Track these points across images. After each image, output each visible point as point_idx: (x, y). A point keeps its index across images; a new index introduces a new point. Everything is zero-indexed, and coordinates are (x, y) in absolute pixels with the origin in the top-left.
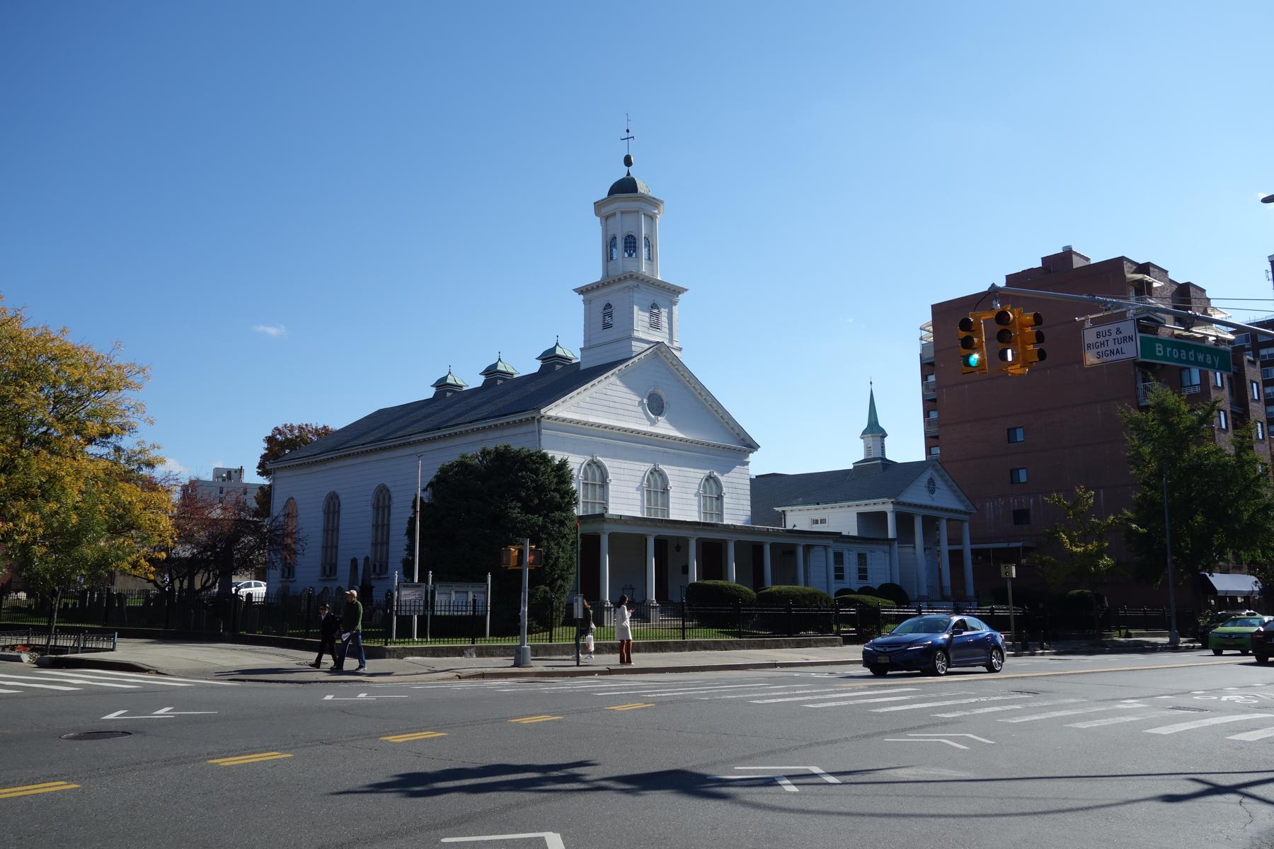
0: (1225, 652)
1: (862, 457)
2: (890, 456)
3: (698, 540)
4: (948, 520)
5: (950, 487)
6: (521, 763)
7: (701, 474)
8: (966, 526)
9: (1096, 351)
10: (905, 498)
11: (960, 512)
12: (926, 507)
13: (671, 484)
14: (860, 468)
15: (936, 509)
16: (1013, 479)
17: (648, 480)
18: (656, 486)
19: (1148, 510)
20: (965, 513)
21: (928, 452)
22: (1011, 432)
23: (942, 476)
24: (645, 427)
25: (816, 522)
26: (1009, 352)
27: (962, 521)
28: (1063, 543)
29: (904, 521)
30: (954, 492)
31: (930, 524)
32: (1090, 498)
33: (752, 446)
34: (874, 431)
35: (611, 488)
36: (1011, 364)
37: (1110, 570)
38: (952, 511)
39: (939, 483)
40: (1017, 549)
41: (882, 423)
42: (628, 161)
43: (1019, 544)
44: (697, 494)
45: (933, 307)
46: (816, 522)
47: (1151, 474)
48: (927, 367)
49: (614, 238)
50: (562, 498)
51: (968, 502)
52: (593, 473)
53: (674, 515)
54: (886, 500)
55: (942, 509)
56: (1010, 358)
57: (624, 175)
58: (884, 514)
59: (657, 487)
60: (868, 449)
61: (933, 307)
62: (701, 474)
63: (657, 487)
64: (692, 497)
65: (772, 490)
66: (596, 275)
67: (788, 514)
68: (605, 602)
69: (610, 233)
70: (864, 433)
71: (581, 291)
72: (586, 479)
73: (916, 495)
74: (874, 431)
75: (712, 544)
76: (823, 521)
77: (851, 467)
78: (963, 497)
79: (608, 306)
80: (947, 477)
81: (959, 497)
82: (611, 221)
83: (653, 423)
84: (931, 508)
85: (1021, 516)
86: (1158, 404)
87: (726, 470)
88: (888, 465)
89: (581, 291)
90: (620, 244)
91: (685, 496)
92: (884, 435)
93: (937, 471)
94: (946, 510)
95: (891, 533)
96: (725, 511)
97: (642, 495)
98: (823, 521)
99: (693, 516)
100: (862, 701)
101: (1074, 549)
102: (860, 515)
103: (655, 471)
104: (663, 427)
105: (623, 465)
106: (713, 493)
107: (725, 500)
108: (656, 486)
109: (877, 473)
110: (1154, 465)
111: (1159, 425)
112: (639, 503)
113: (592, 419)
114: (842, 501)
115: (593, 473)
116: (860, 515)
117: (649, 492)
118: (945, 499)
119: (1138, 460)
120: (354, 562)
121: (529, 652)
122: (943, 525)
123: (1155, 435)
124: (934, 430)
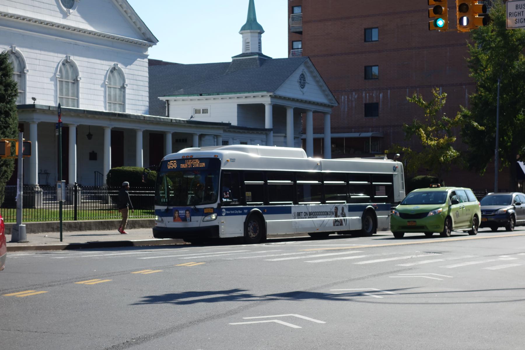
1: (240, 52)
2: (265, 52)
3: (145, 133)
4: (314, 112)
5: (317, 82)
6: (205, 291)
7: (106, 65)
8: (328, 118)
9: (514, 18)
10: (281, 92)
11: (324, 105)
12: (297, 100)
13: (80, 75)
14: (239, 63)
16: (367, 74)
17: (61, 71)
18: (67, 77)
19: (483, 109)
20: (328, 106)
21: (291, 47)
22: (367, 31)
23: (311, 72)
24: (58, 20)
25: (197, 111)
26: (465, 19)
27: (325, 113)
28: (420, 137)
29: (279, 113)
30: (320, 87)
31: (299, 113)
32: (441, 97)
33: (152, 40)
34: (253, 27)
35: (81, 85)
36: (465, 27)
37: (455, 160)
38: (317, 104)
40: (367, 138)
41: (259, 20)
43: (369, 134)
44: (104, 85)
46: (197, 111)
47: (487, 78)
50: (6, 90)
51: (331, 97)
52: (67, 72)
53: (83, 106)
54: (265, 93)
55: (310, 103)
56: (465, 23)
58: (261, 107)
59: (68, 77)
60: (246, 44)
62: (106, 65)
63: (68, 77)
64: (99, 87)
65: (168, 78)
67: (172, 104)
68: (35, 186)
70: (244, 28)
72: (62, 77)
73: (290, 89)
74: (253, 27)
75: (121, 132)
76: (205, 111)
77: (230, 60)
78: (328, 92)
80: (316, 73)
81: (324, 91)
83: (65, 15)
85: (371, 109)
86: (498, 18)
87: (128, 62)
88: (264, 60)
91: (93, 87)
92: (260, 31)
93: (308, 67)
94: (293, 100)
95: (268, 124)
96: (127, 101)
97: (56, 85)
98: (205, 111)
99: (100, 107)
100: (339, 259)
101: (430, 142)
102: (241, 107)
103: (67, 62)
104: (75, 20)
105: (39, 57)
106: (116, 82)
107: (127, 91)
108: (67, 77)
109: (250, 69)
110: (490, 70)
111: (498, 36)
112: (53, 93)
113: (11, 11)
114: (223, 92)
115: (67, 72)
116: (241, 107)
117: (61, 82)
118: (314, 93)
119: (476, 64)
121: (25, 230)
122: (310, 117)
123: (493, 45)
124: (298, 26)
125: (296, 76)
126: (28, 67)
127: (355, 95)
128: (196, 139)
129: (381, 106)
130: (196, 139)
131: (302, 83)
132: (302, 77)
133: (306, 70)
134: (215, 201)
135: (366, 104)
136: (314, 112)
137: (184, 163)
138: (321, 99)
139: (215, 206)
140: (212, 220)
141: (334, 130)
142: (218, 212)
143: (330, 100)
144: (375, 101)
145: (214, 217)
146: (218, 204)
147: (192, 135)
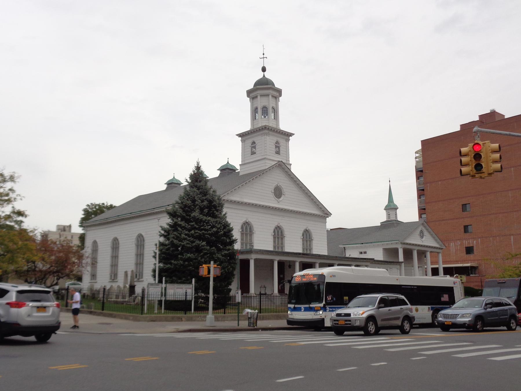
0: (451, 330)
2: (399, 219)
4: (431, 252)
12: (419, 245)
14: (385, 225)
15: (424, 246)
20: (440, 248)
21: (420, 217)
27: (438, 253)
29: (408, 254)
33: (326, 214)
38: (432, 247)
39: (426, 233)
42: (264, 70)
43: (468, 265)
45: (422, 141)
46: (361, 253)
48: (420, 173)
49: (257, 108)
57: (262, 76)
61: (422, 141)
63: (279, 234)
66: (247, 127)
69: (255, 106)
71: (241, 135)
73: (415, 240)
76: (365, 253)
79: (254, 143)
82: (255, 100)
84: (422, 246)
85: (469, 250)
89: (241, 135)
90: (260, 111)
93: (425, 227)
94: (430, 247)
95: (401, 258)
118: (429, 241)
120: (126, 273)
125: (418, 231)
126: (255, 229)
127: (459, 242)
128: (317, 265)
129: (475, 248)
130: (317, 265)
131: (422, 235)
132: (422, 232)
133: (423, 228)
134: (322, 302)
135: (466, 248)
136: (431, 252)
137: (305, 278)
138: (434, 244)
139: (322, 305)
140: (320, 314)
141: (444, 263)
142: (324, 309)
143: (440, 245)
144: (471, 245)
145: (321, 313)
146: (324, 304)
147: (315, 263)
